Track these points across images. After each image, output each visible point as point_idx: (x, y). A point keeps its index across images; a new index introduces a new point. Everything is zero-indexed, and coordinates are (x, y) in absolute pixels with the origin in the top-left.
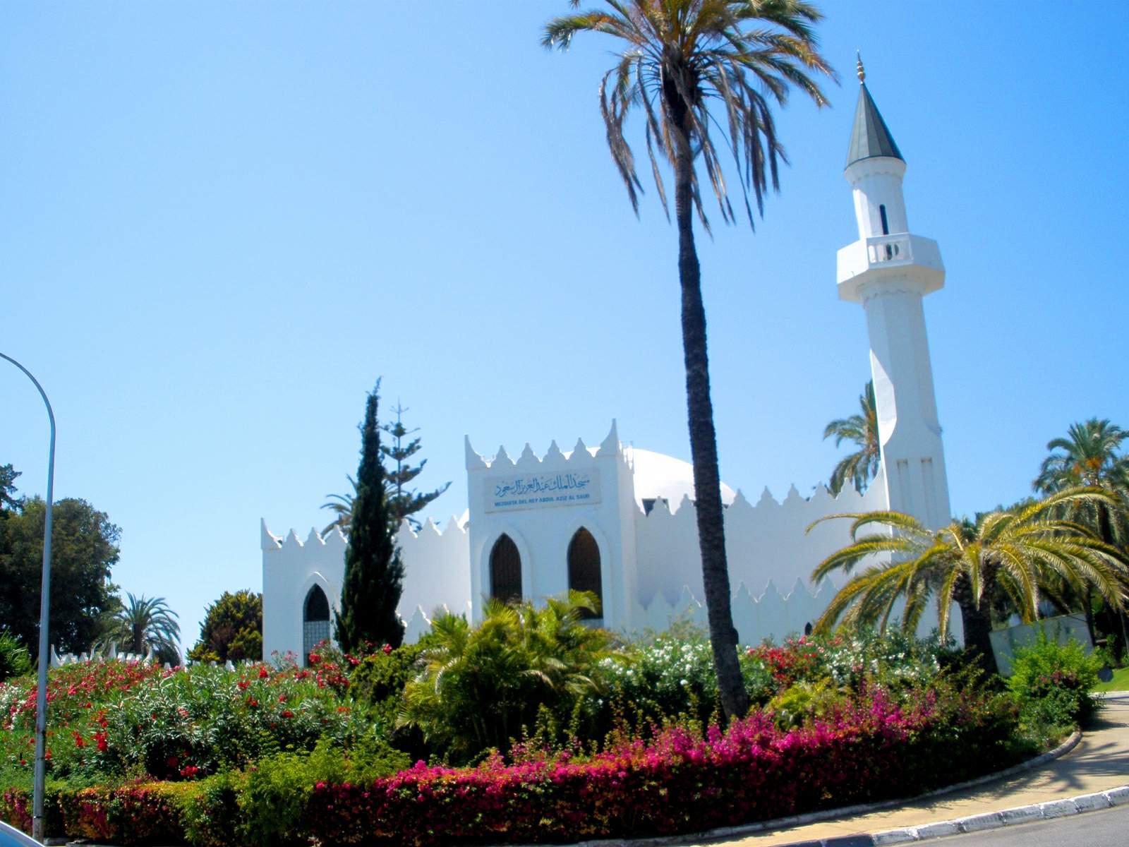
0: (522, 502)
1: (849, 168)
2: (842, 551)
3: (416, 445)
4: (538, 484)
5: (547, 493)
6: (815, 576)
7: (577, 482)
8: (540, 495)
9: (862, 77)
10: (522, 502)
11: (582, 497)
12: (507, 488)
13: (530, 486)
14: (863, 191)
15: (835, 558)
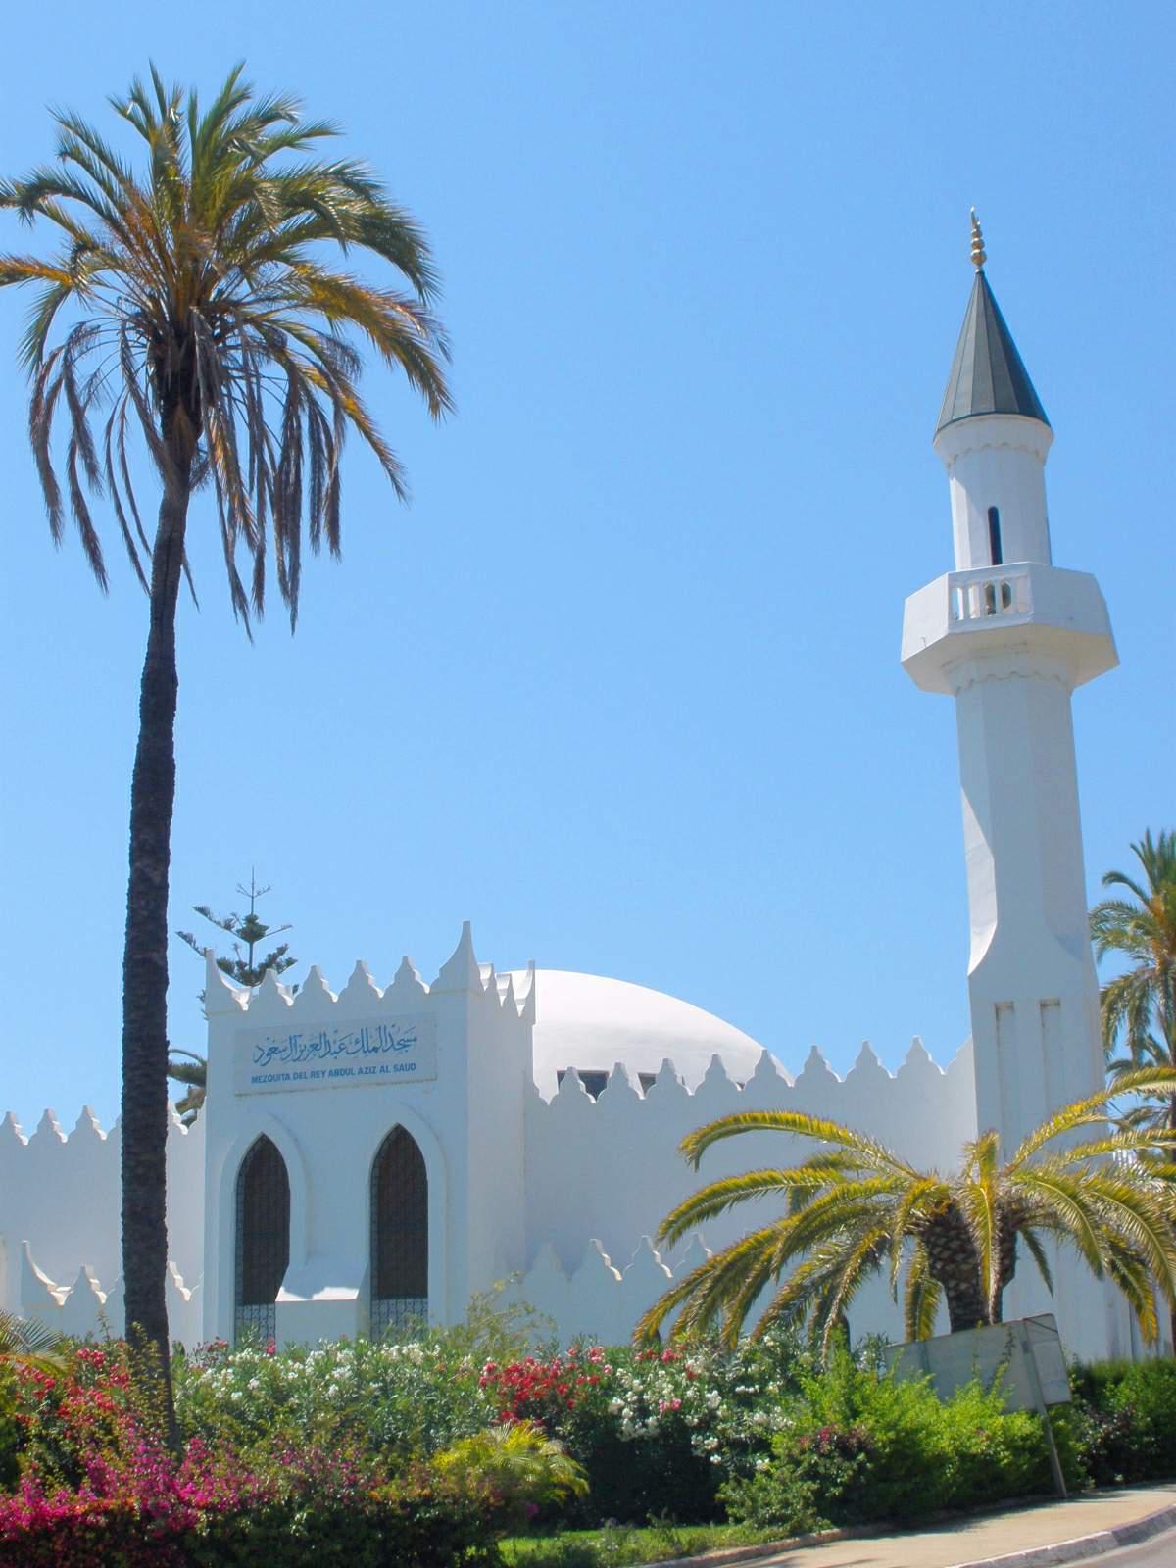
0: (299, 1076)
1: (938, 436)
2: (716, 1186)
3: (283, 958)
4: (327, 1042)
5: (343, 1061)
6: (666, 1231)
7: (396, 1039)
8: (330, 1064)
9: (980, 259)
10: (299, 1076)
11: (402, 1068)
12: (274, 1050)
13: (314, 1047)
14: (965, 482)
15: (703, 1200)
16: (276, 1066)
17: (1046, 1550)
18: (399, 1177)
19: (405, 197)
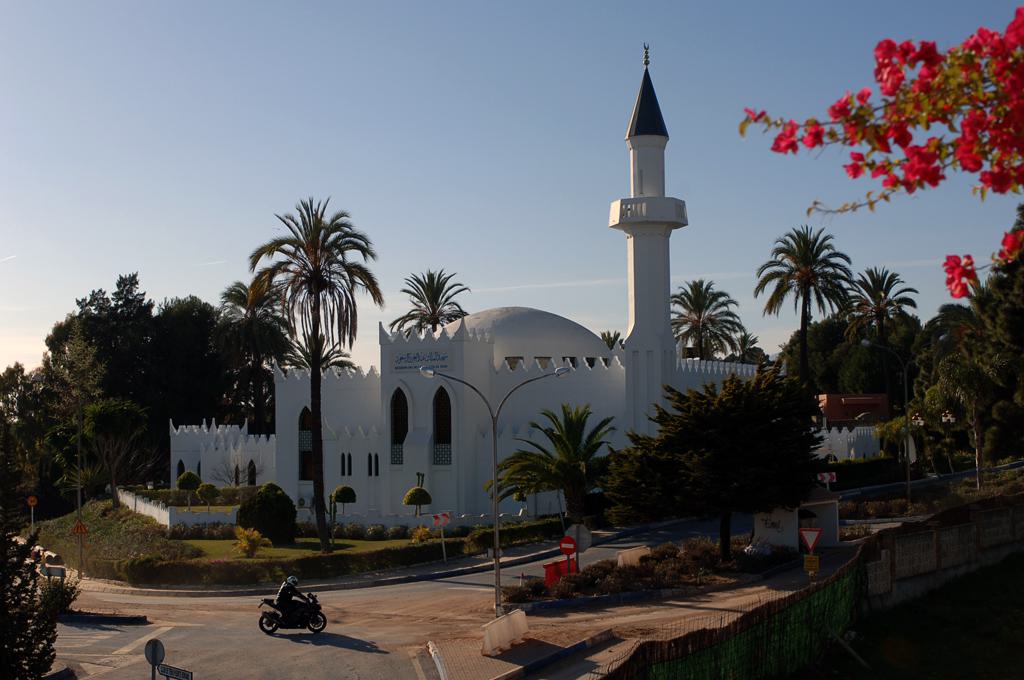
9: (647, 63)
12: (402, 358)
16: (403, 364)
17: (584, 642)
18: (442, 402)
19: (725, 291)
